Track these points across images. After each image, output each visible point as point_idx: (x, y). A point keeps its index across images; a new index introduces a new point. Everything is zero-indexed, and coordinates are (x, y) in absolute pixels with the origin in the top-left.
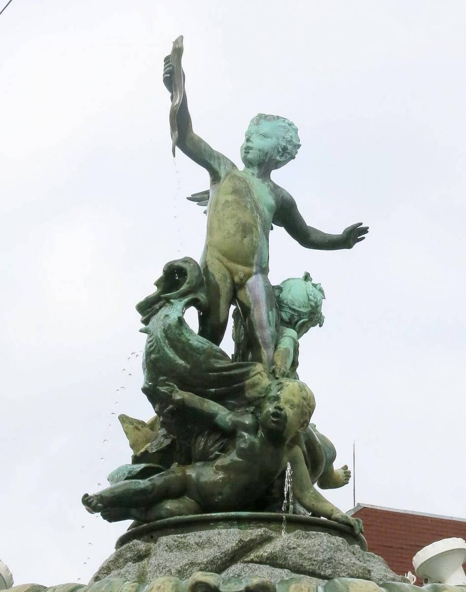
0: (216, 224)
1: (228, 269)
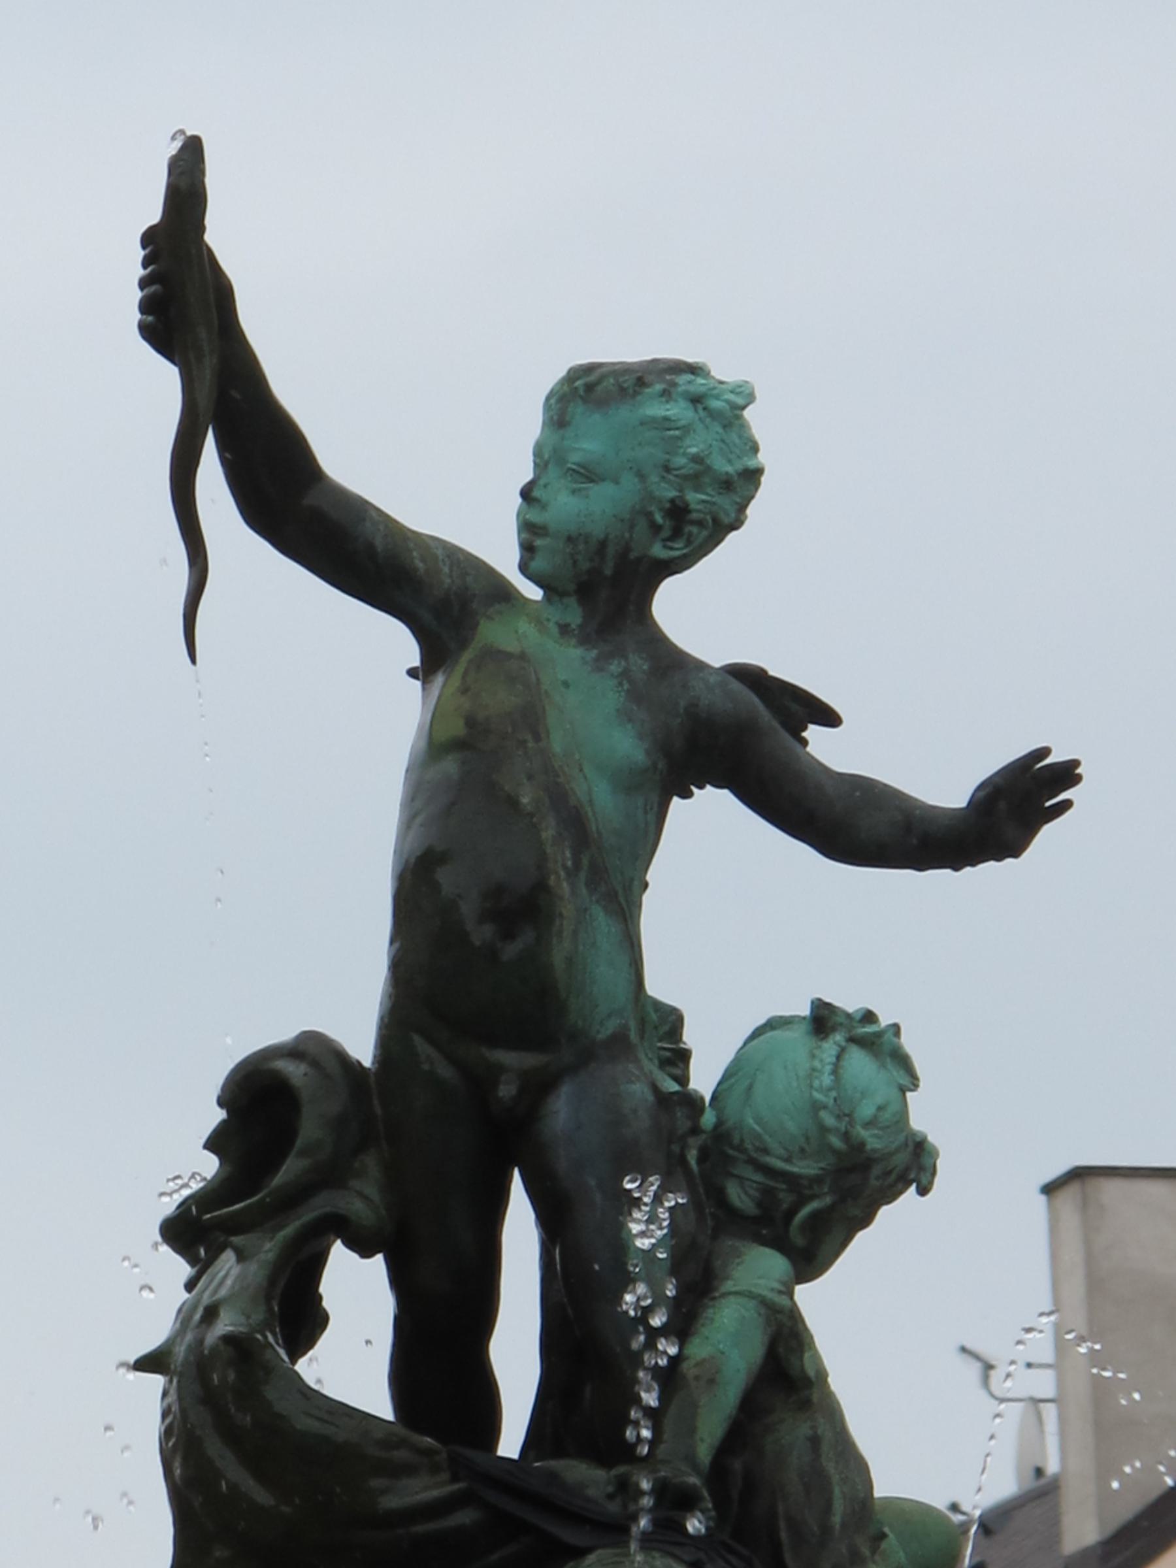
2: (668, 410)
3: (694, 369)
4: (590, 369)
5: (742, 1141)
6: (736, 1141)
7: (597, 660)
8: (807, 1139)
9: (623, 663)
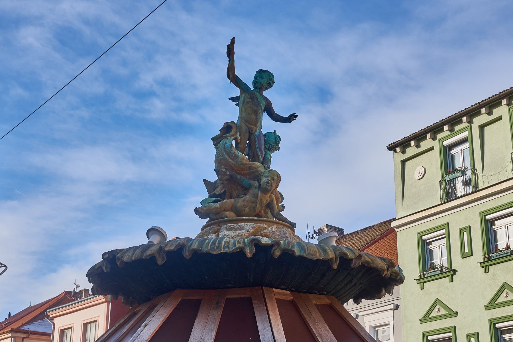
0: (243, 110)
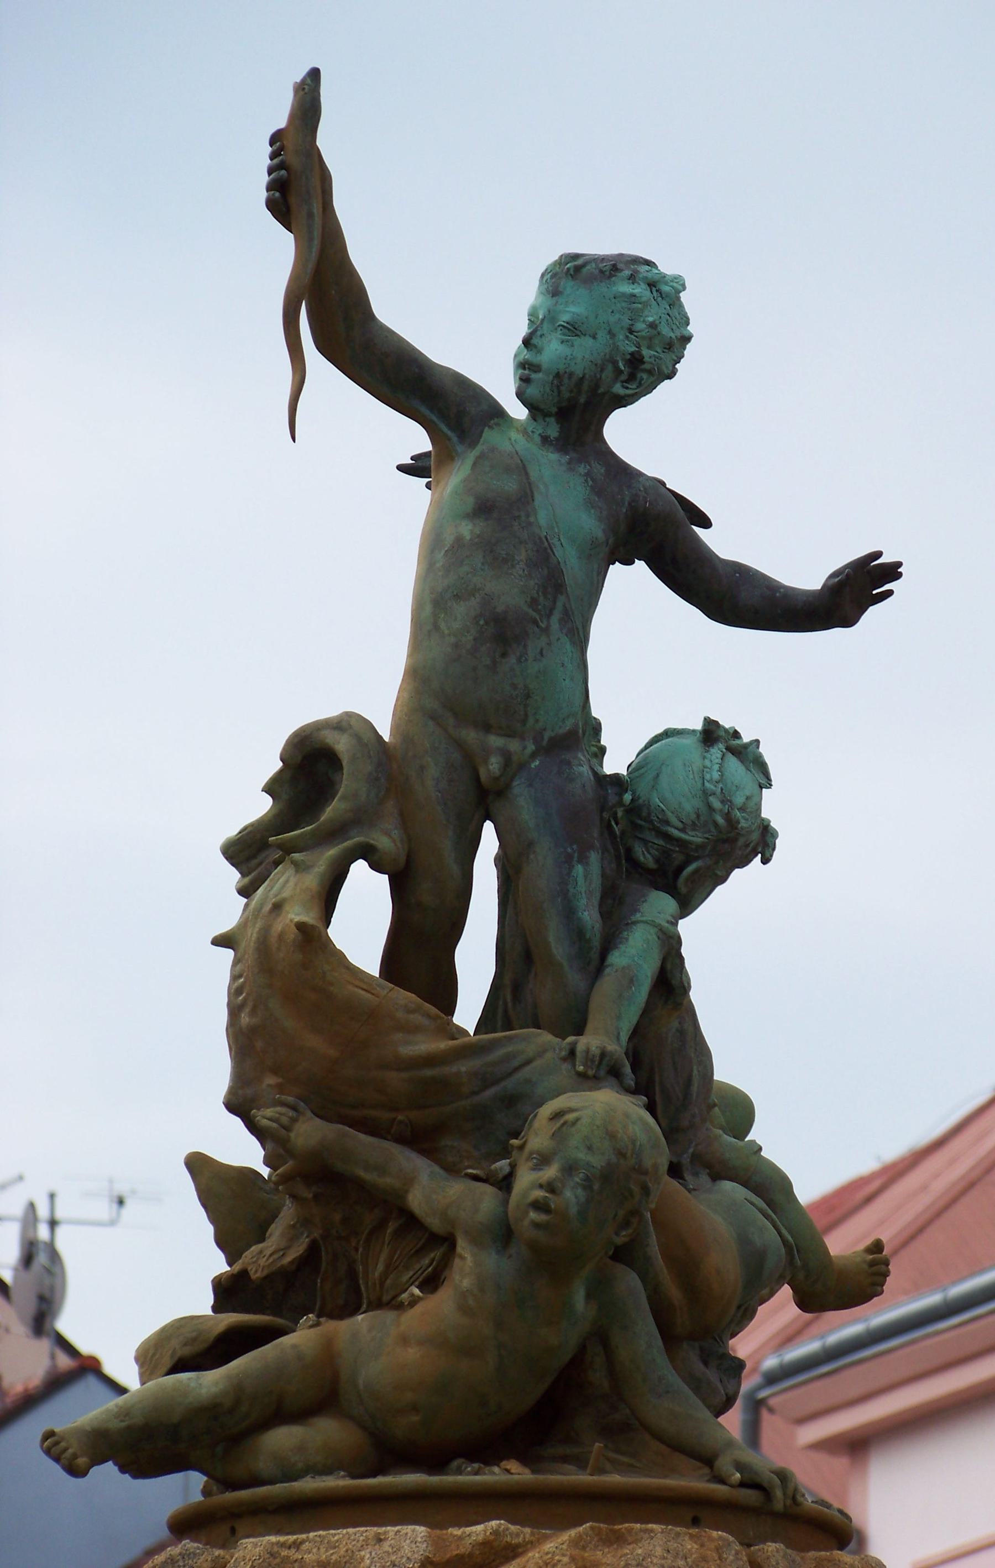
1: (459, 745)
2: (633, 289)
3: (648, 263)
4: (576, 257)
5: (649, 814)
6: (644, 814)
7: (569, 463)
8: (698, 816)
9: (588, 467)
